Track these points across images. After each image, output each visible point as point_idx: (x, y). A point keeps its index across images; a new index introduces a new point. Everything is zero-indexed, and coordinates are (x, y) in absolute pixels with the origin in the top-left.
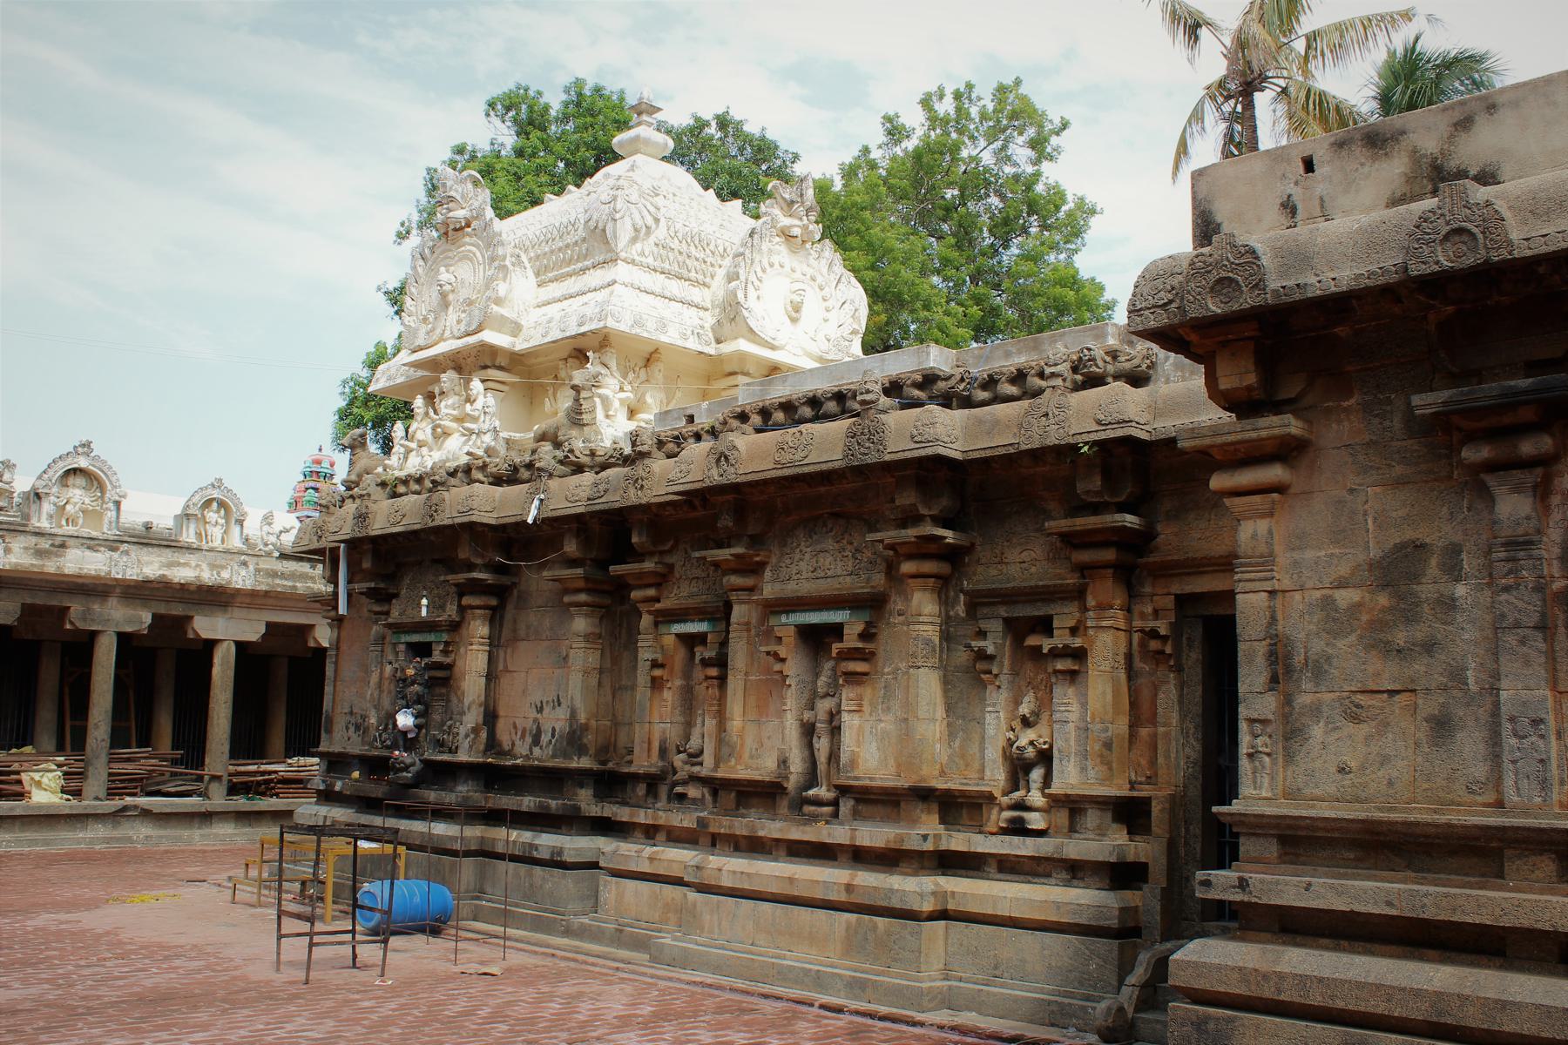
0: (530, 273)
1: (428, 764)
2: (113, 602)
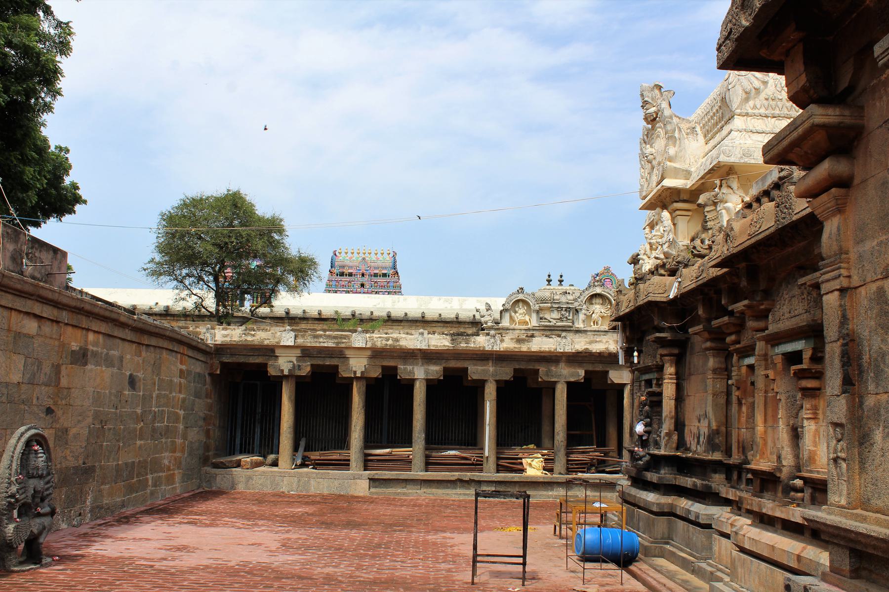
0: (701, 137)
1: (653, 456)
2: (562, 364)
